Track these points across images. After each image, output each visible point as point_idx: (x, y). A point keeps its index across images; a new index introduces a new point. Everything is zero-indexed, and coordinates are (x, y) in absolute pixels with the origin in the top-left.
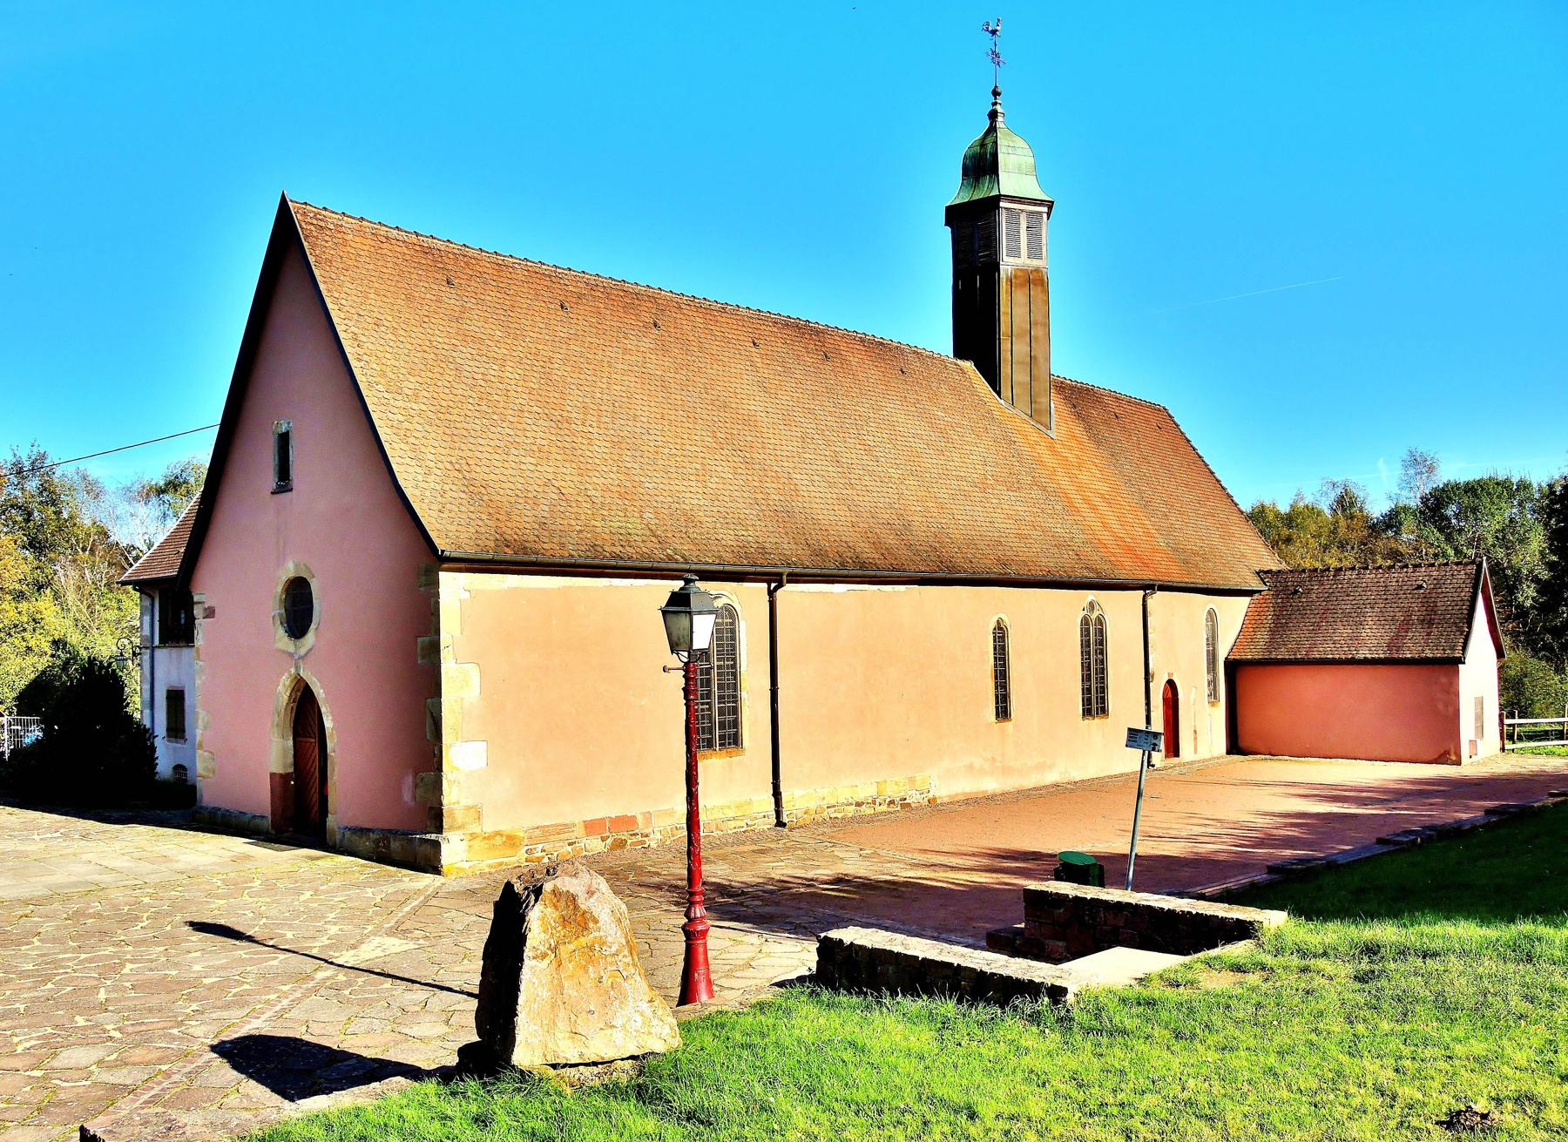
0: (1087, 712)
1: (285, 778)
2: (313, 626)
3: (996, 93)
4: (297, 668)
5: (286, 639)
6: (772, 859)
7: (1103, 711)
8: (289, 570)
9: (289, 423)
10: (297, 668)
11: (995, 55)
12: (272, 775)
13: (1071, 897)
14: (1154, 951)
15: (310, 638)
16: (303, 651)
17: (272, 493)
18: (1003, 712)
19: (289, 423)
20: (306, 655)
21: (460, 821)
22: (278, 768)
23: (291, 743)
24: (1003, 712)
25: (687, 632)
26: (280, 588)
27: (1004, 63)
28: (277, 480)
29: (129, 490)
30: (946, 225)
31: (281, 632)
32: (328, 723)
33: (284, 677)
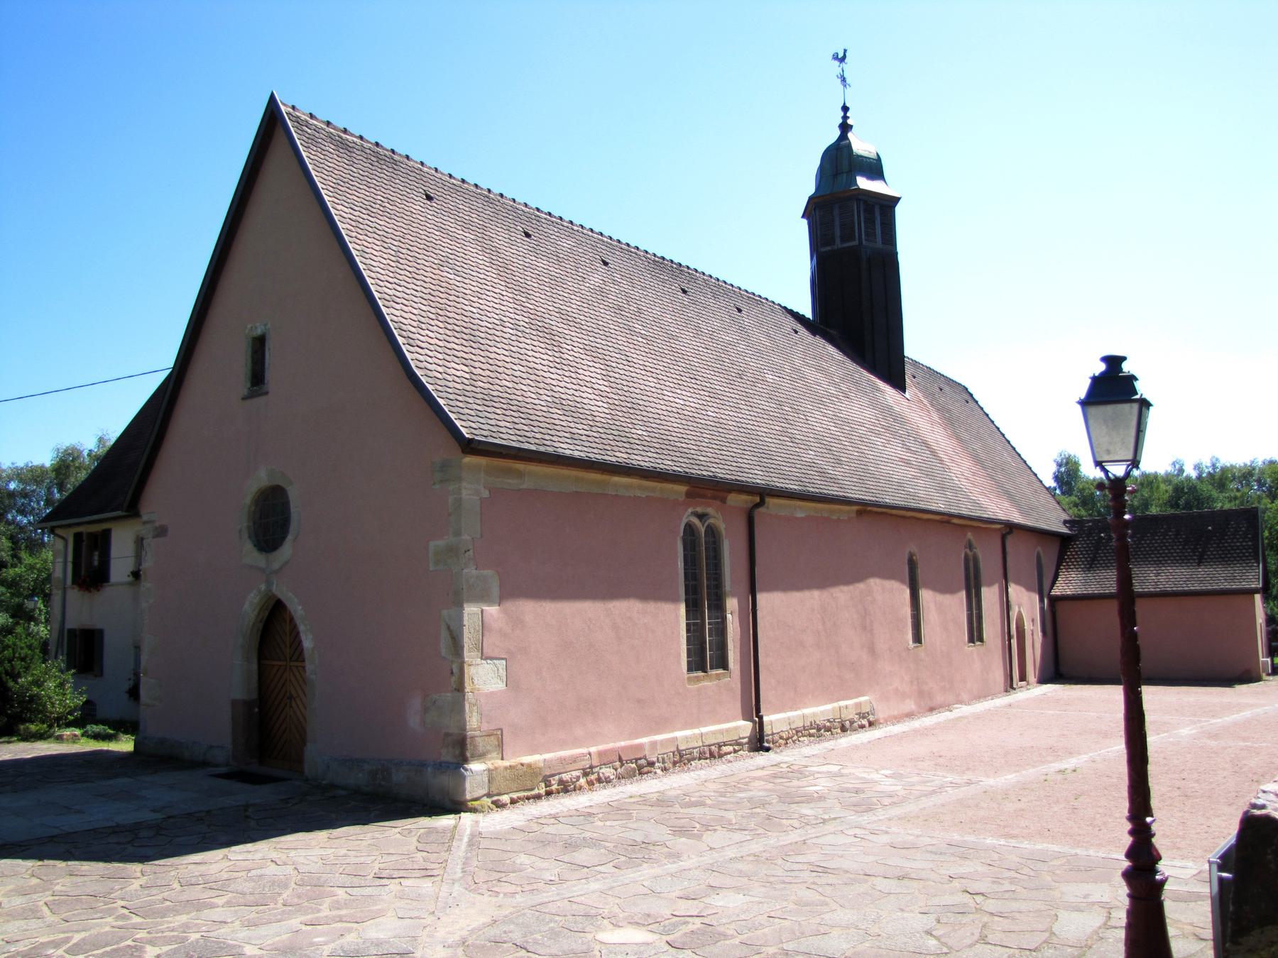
0: (971, 640)
1: (248, 704)
2: (290, 537)
3: (845, 109)
4: (269, 583)
5: (255, 553)
6: (843, 785)
7: (981, 639)
8: (261, 479)
9: (265, 325)
10: (269, 583)
11: (843, 80)
12: (234, 703)
13: (1149, 819)
14: (408, 818)
15: (286, 550)
16: (276, 566)
17: (244, 399)
18: (917, 638)
19: (265, 325)
20: (281, 568)
21: (481, 749)
22: (239, 694)
23: (255, 667)
24: (917, 638)
25: (1091, 422)
26: (248, 500)
27: (849, 85)
28: (249, 385)
29: (58, 449)
30: (803, 217)
31: (249, 546)
32: (307, 643)
33: (252, 595)
